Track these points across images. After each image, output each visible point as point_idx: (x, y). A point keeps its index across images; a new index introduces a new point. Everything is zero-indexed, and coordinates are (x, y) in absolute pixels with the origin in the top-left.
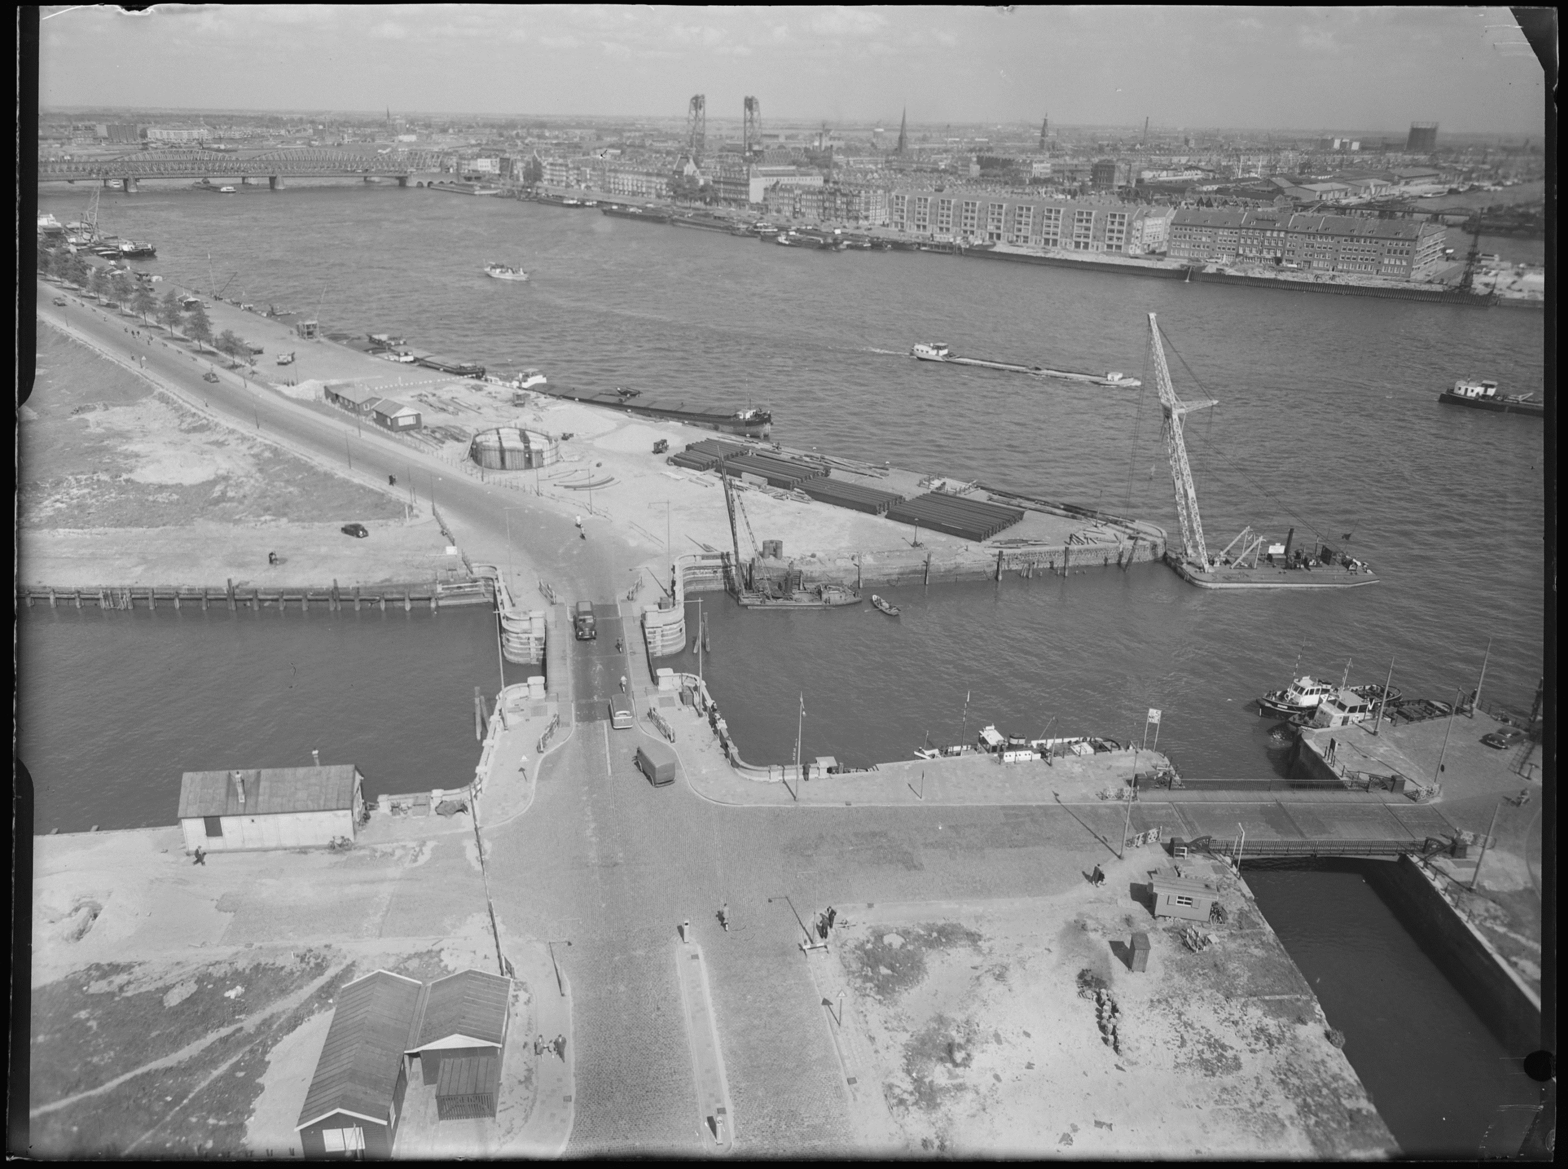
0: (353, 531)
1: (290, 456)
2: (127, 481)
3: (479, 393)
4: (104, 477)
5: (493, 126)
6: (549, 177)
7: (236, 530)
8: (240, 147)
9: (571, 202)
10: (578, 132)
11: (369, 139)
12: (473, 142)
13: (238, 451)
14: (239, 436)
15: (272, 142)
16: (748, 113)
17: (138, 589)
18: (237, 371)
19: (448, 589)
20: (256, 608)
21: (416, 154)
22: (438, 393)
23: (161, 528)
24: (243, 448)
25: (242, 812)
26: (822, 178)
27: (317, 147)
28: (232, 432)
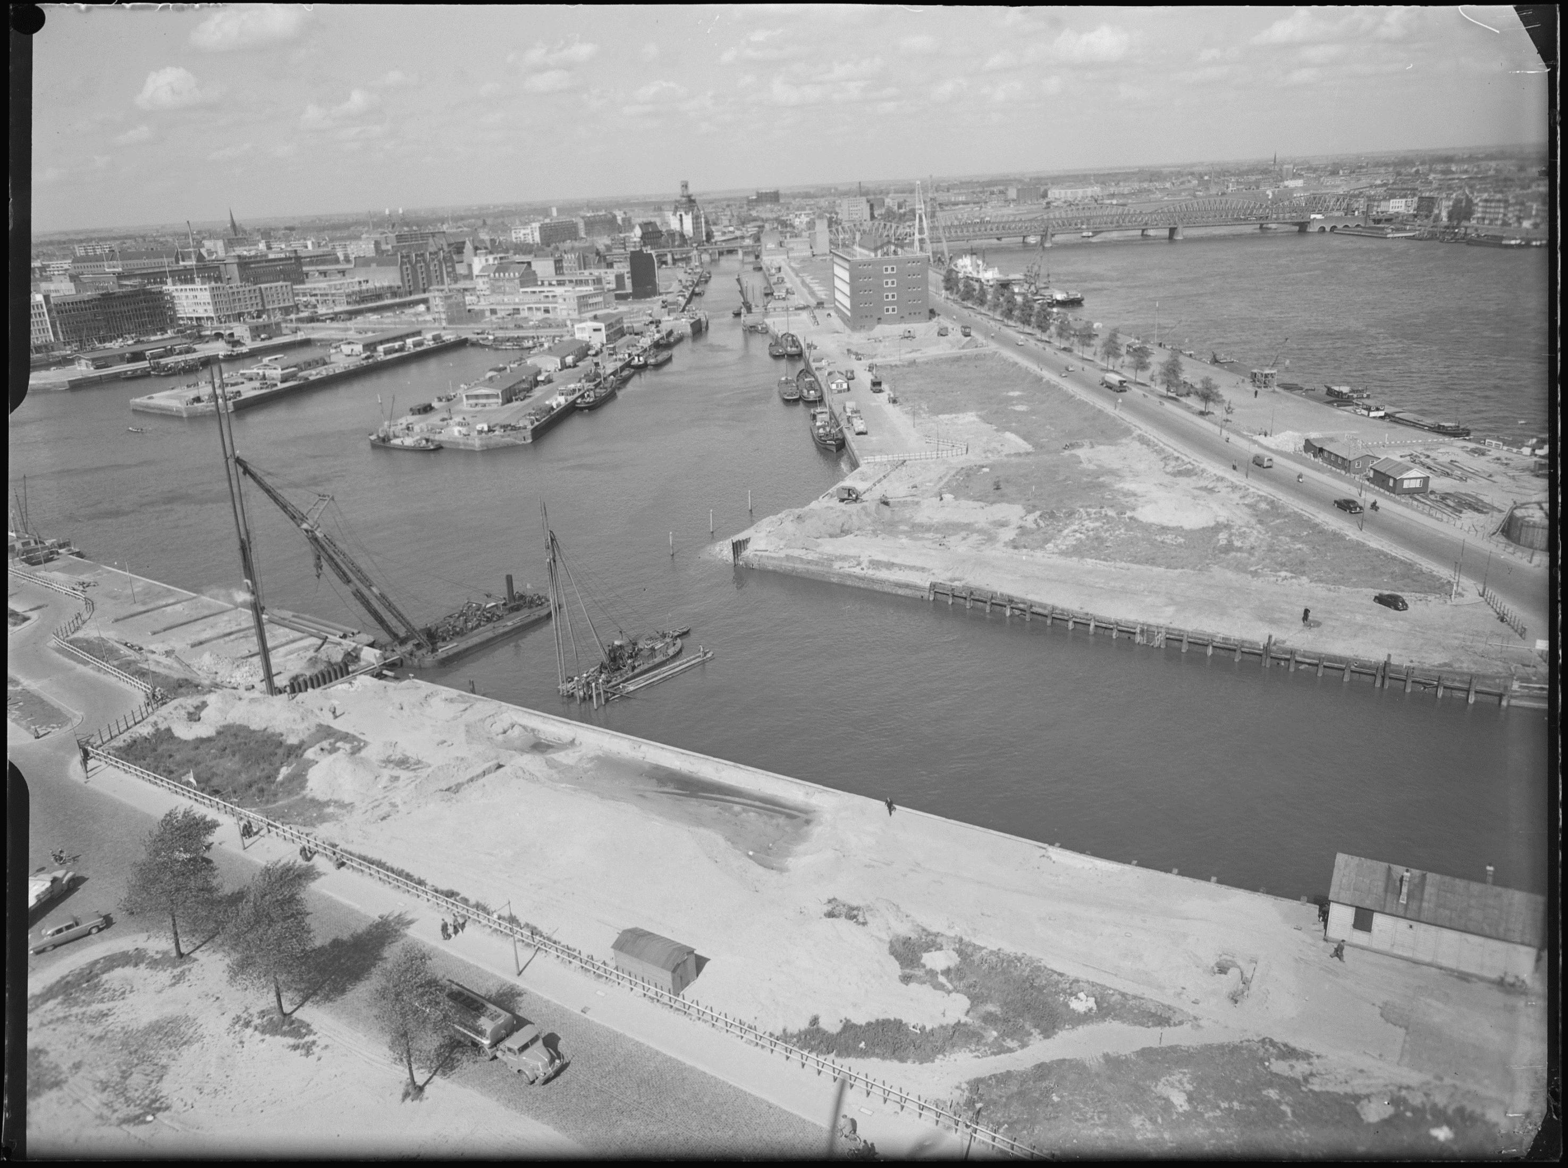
0: (1391, 602)
1: (1289, 510)
2: (1131, 518)
3: (1482, 458)
4: (1111, 513)
5: (1387, 165)
6: (1479, 215)
7: (1256, 583)
8: (1130, 201)
9: (1513, 242)
10: (1493, 164)
11: (1253, 187)
12: (1378, 182)
13: (1231, 500)
14: (1229, 484)
15: (1158, 195)
17: (1174, 629)
18: (1207, 417)
19: (1527, 688)
20: (1292, 669)
21: (1320, 199)
22: (1433, 454)
23: (1179, 570)
24: (1236, 496)
25: (1402, 914)
27: (1201, 197)
28: (1221, 479)
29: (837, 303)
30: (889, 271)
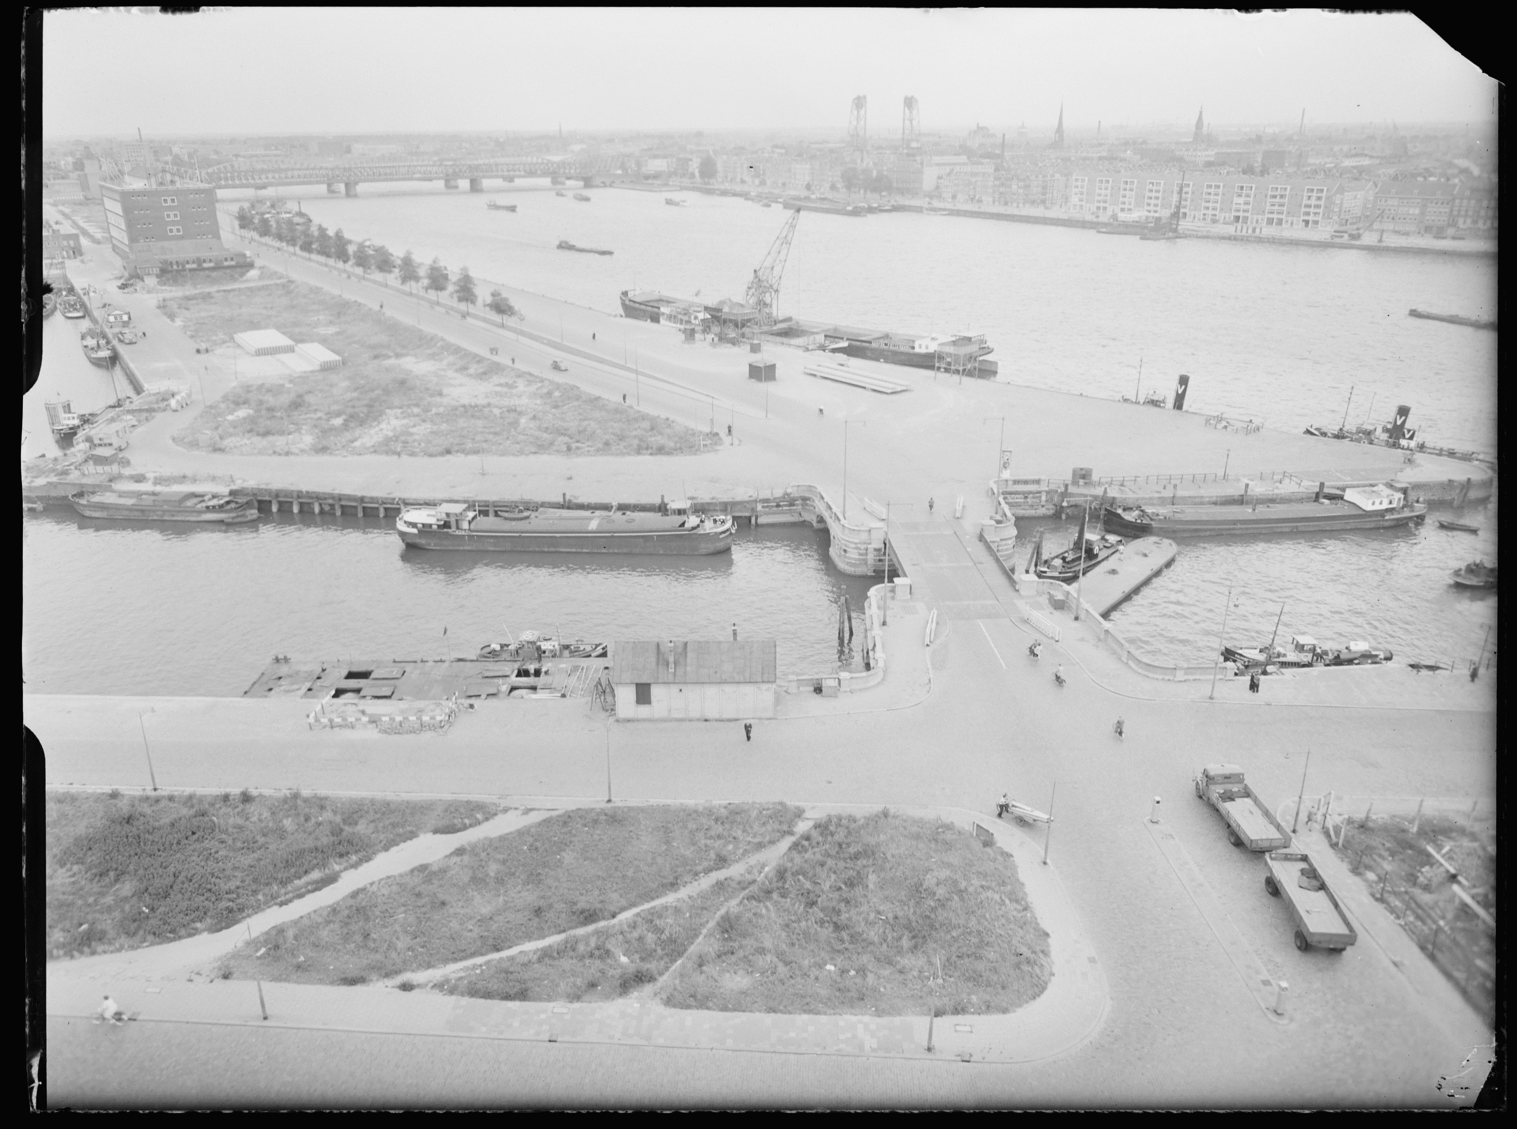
16: (907, 111)
19: (767, 507)
26: (993, 167)
29: (115, 242)
30: (169, 199)
